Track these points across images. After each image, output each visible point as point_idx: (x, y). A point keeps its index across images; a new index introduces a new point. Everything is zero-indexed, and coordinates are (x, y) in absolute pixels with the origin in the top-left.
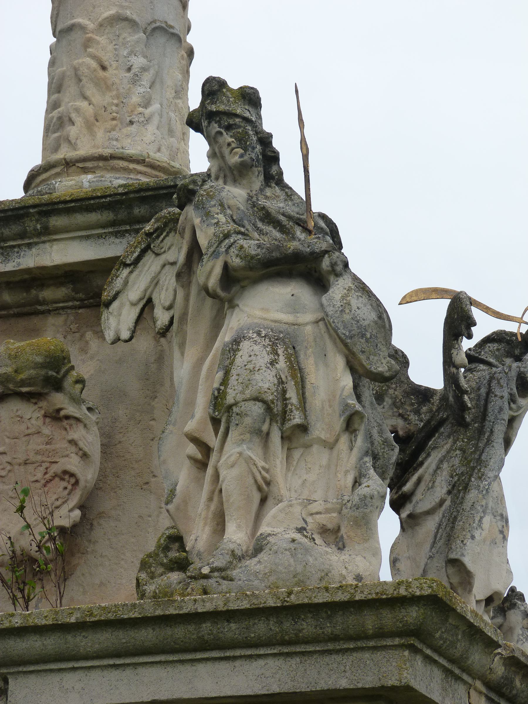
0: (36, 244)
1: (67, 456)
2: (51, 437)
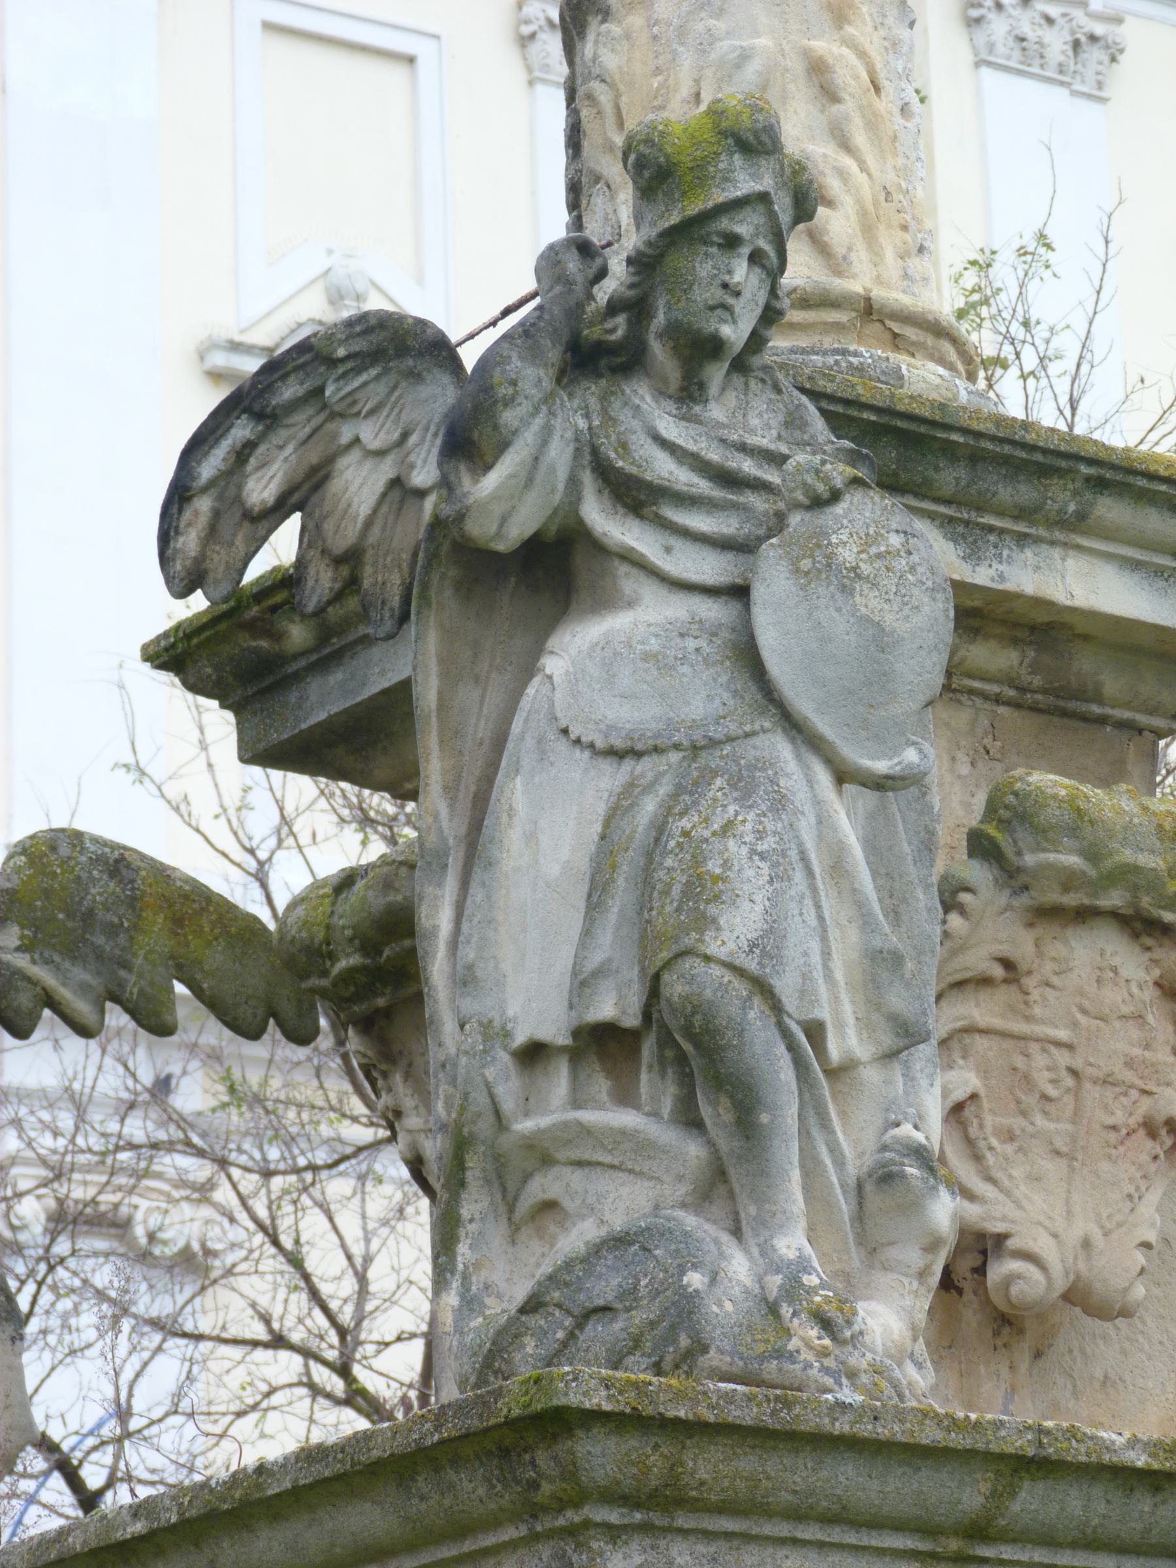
0: (1038, 540)
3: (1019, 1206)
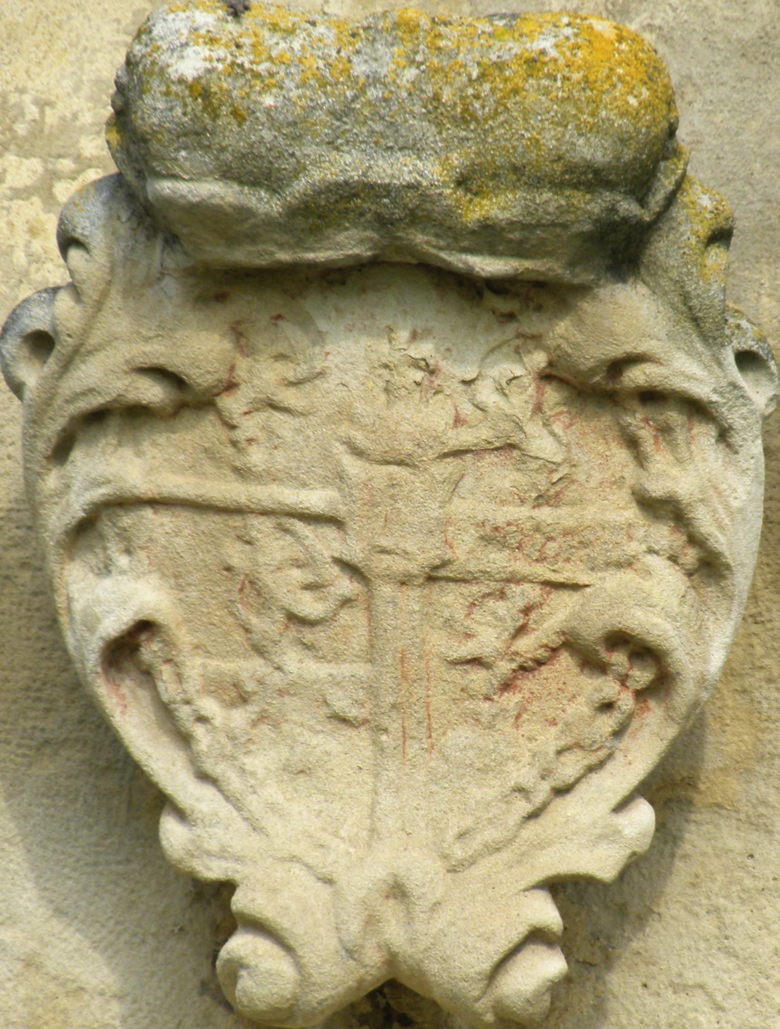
1: (626, 564)
2: (564, 471)
3: (256, 827)
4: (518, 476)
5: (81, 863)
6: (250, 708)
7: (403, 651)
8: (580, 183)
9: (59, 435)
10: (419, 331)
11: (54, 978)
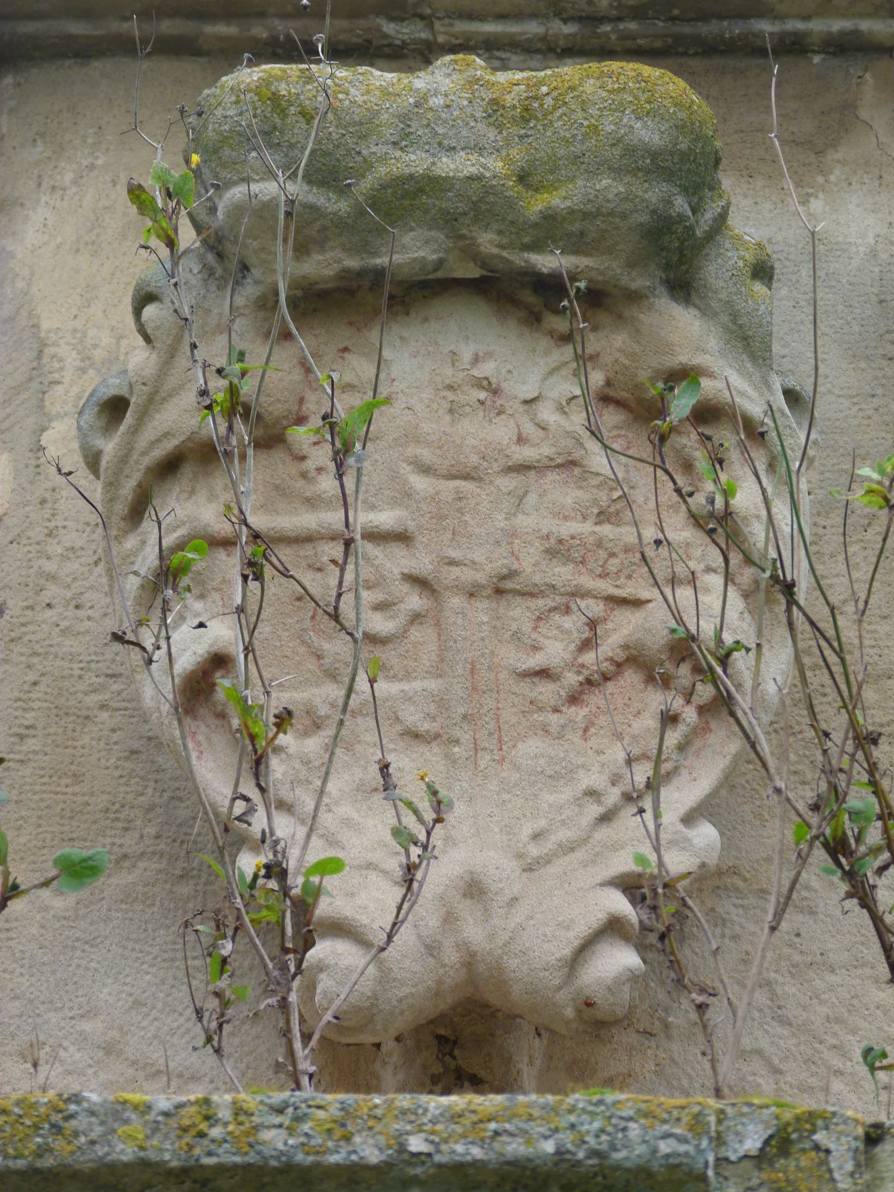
4: (580, 493)
5: (159, 959)
6: (323, 733)
7: (473, 662)
8: (639, 169)
9: (135, 491)
10: (481, 354)
11: (134, 1063)
